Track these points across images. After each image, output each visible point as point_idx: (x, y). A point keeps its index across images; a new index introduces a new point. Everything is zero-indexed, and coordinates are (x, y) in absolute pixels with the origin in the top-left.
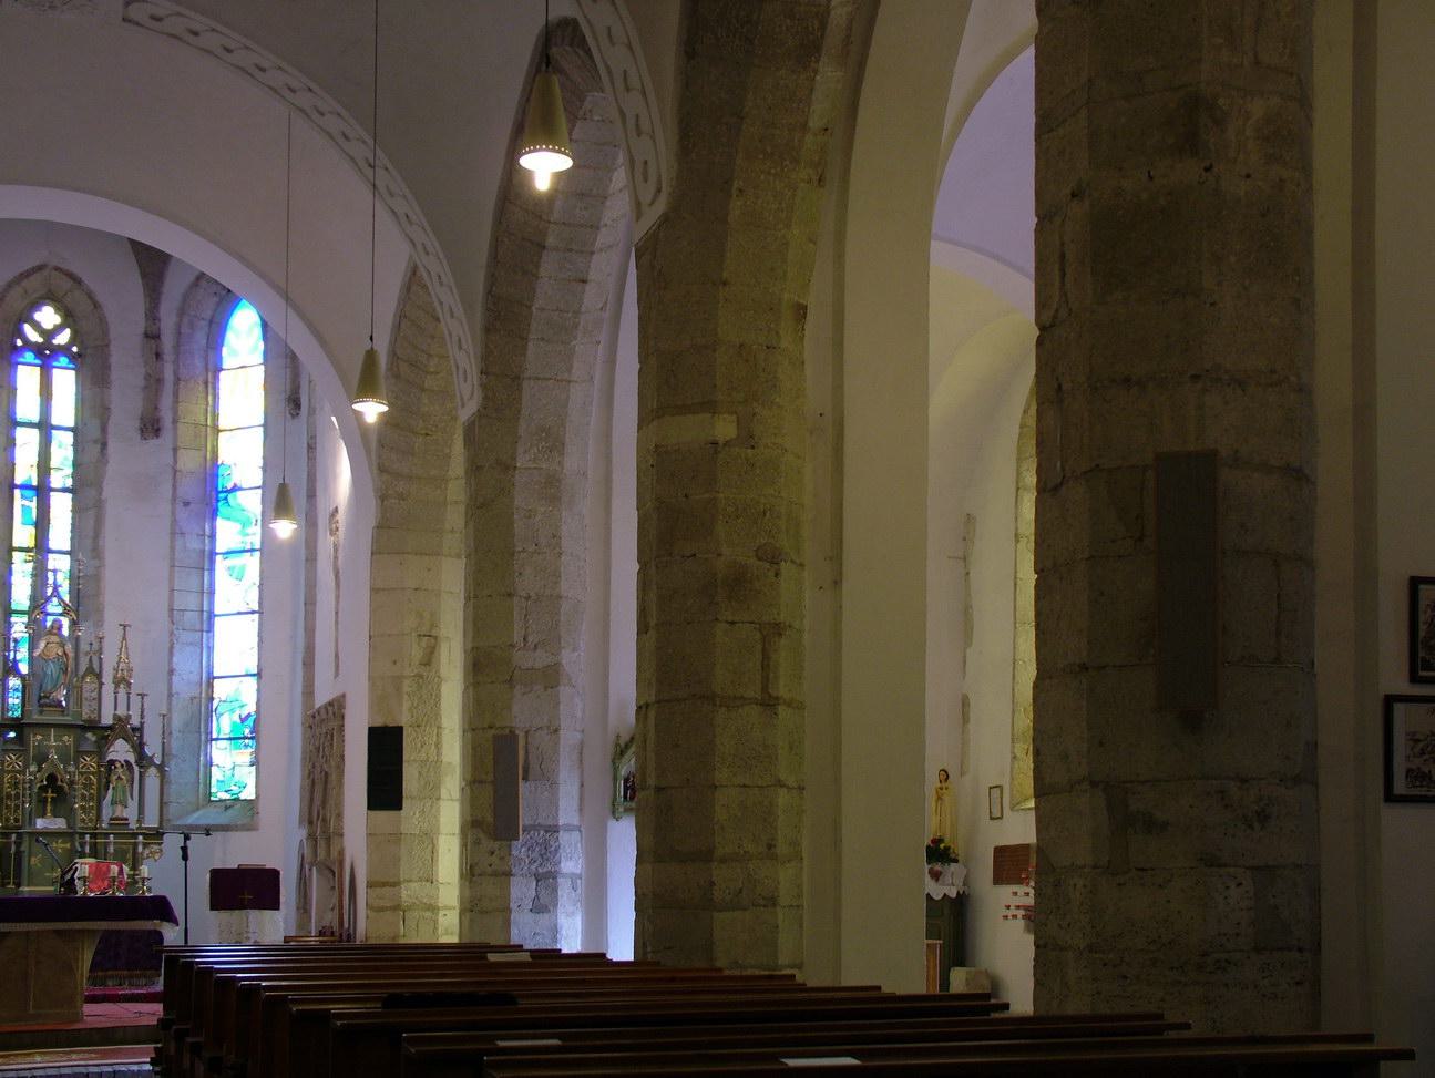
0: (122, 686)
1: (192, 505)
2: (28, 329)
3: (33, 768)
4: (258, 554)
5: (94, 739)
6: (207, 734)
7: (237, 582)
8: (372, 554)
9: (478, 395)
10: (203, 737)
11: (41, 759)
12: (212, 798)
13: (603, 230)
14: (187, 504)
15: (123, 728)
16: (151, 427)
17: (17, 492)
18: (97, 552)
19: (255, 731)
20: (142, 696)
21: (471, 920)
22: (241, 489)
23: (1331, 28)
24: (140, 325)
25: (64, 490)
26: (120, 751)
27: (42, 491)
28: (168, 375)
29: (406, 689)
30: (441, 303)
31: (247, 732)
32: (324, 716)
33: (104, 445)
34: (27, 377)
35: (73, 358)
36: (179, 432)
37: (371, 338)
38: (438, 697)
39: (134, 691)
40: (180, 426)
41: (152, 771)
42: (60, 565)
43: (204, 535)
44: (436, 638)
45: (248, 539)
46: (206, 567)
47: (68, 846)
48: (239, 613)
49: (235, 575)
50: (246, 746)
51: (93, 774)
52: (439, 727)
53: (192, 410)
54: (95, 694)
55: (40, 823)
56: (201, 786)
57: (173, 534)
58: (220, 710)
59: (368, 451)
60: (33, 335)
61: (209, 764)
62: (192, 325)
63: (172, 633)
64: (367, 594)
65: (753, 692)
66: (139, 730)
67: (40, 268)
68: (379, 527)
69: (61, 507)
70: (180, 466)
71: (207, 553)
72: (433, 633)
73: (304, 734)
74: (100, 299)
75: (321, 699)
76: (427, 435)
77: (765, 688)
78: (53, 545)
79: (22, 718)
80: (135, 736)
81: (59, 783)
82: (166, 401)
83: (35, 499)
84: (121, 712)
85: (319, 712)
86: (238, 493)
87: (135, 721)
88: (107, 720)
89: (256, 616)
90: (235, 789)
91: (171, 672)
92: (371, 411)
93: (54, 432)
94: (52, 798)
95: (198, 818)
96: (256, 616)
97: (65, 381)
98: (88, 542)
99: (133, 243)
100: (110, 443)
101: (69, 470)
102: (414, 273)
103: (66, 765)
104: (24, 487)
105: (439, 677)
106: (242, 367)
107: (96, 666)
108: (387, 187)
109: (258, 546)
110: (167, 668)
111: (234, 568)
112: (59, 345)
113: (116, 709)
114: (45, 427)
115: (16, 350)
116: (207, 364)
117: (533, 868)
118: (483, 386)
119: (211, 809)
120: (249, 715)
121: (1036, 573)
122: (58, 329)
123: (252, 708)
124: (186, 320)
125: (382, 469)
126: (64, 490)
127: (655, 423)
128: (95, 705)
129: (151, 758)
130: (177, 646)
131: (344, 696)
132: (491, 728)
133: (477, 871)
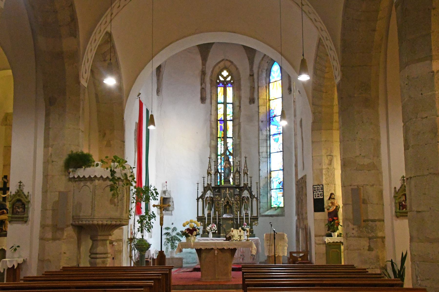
0: (245, 175)
1: (264, 122)
2: (220, 77)
3: (223, 200)
4: (281, 134)
5: (238, 190)
6: (270, 188)
8: (312, 131)
9: (340, 74)
11: (225, 197)
12: (272, 207)
13: (380, 12)
14: (262, 122)
15: (246, 187)
16: (252, 101)
17: (219, 122)
18: (239, 137)
19: (284, 186)
20: (251, 177)
21: (347, 253)
22: (277, 116)
24: (248, 72)
25: (230, 120)
26: (246, 194)
27: (225, 121)
28: (256, 86)
30: (327, 46)
31: (281, 187)
32: (301, 182)
33: (240, 107)
34: (220, 90)
35: (232, 84)
37: (303, 55)
38: (334, 175)
39: (249, 176)
40: (259, 100)
41: (255, 199)
42: (230, 142)
43: (267, 130)
44: (332, 156)
46: (268, 139)
47: (232, 222)
48: (277, 152)
50: (281, 191)
52: (335, 184)
53: (263, 95)
54: (238, 178)
55: (225, 216)
57: (259, 130)
58: (273, 181)
59: (308, 97)
60: (222, 79)
61: (271, 197)
62: (262, 72)
63: (259, 159)
66: (250, 188)
67: (223, 60)
68: (313, 122)
69: (230, 124)
70: (260, 111)
71: (268, 136)
72: (332, 154)
73: (296, 187)
74: (238, 67)
75: (300, 177)
76: (326, 92)
78: (228, 136)
79: (220, 185)
80: (250, 190)
81: (230, 204)
82: (256, 94)
83: (223, 123)
84: (246, 182)
85: (299, 181)
86: (276, 117)
87: (249, 186)
89: (282, 152)
90: (278, 204)
91: (260, 170)
92: (304, 78)
93: (227, 104)
94: (228, 208)
96: (282, 152)
97: (230, 90)
98: (237, 134)
99: (245, 47)
100: (242, 107)
101: (232, 115)
102: (319, 41)
103: (231, 198)
104: (220, 120)
105: (334, 168)
106: (275, 81)
107: (239, 169)
108: (309, 11)
109: (282, 132)
111: (275, 139)
112: (228, 81)
113: (244, 182)
114: (225, 103)
115: (218, 84)
116: (266, 81)
118: (342, 71)
119: (272, 210)
120: (281, 182)
121: (112, 204)
122: (228, 76)
123: (282, 180)
124: (260, 70)
125: (313, 104)
126: (230, 120)
127: (407, 67)
128: (238, 181)
130: (261, 162)
131: (306, 175)
132: (351, 186)
133: (349, 235)
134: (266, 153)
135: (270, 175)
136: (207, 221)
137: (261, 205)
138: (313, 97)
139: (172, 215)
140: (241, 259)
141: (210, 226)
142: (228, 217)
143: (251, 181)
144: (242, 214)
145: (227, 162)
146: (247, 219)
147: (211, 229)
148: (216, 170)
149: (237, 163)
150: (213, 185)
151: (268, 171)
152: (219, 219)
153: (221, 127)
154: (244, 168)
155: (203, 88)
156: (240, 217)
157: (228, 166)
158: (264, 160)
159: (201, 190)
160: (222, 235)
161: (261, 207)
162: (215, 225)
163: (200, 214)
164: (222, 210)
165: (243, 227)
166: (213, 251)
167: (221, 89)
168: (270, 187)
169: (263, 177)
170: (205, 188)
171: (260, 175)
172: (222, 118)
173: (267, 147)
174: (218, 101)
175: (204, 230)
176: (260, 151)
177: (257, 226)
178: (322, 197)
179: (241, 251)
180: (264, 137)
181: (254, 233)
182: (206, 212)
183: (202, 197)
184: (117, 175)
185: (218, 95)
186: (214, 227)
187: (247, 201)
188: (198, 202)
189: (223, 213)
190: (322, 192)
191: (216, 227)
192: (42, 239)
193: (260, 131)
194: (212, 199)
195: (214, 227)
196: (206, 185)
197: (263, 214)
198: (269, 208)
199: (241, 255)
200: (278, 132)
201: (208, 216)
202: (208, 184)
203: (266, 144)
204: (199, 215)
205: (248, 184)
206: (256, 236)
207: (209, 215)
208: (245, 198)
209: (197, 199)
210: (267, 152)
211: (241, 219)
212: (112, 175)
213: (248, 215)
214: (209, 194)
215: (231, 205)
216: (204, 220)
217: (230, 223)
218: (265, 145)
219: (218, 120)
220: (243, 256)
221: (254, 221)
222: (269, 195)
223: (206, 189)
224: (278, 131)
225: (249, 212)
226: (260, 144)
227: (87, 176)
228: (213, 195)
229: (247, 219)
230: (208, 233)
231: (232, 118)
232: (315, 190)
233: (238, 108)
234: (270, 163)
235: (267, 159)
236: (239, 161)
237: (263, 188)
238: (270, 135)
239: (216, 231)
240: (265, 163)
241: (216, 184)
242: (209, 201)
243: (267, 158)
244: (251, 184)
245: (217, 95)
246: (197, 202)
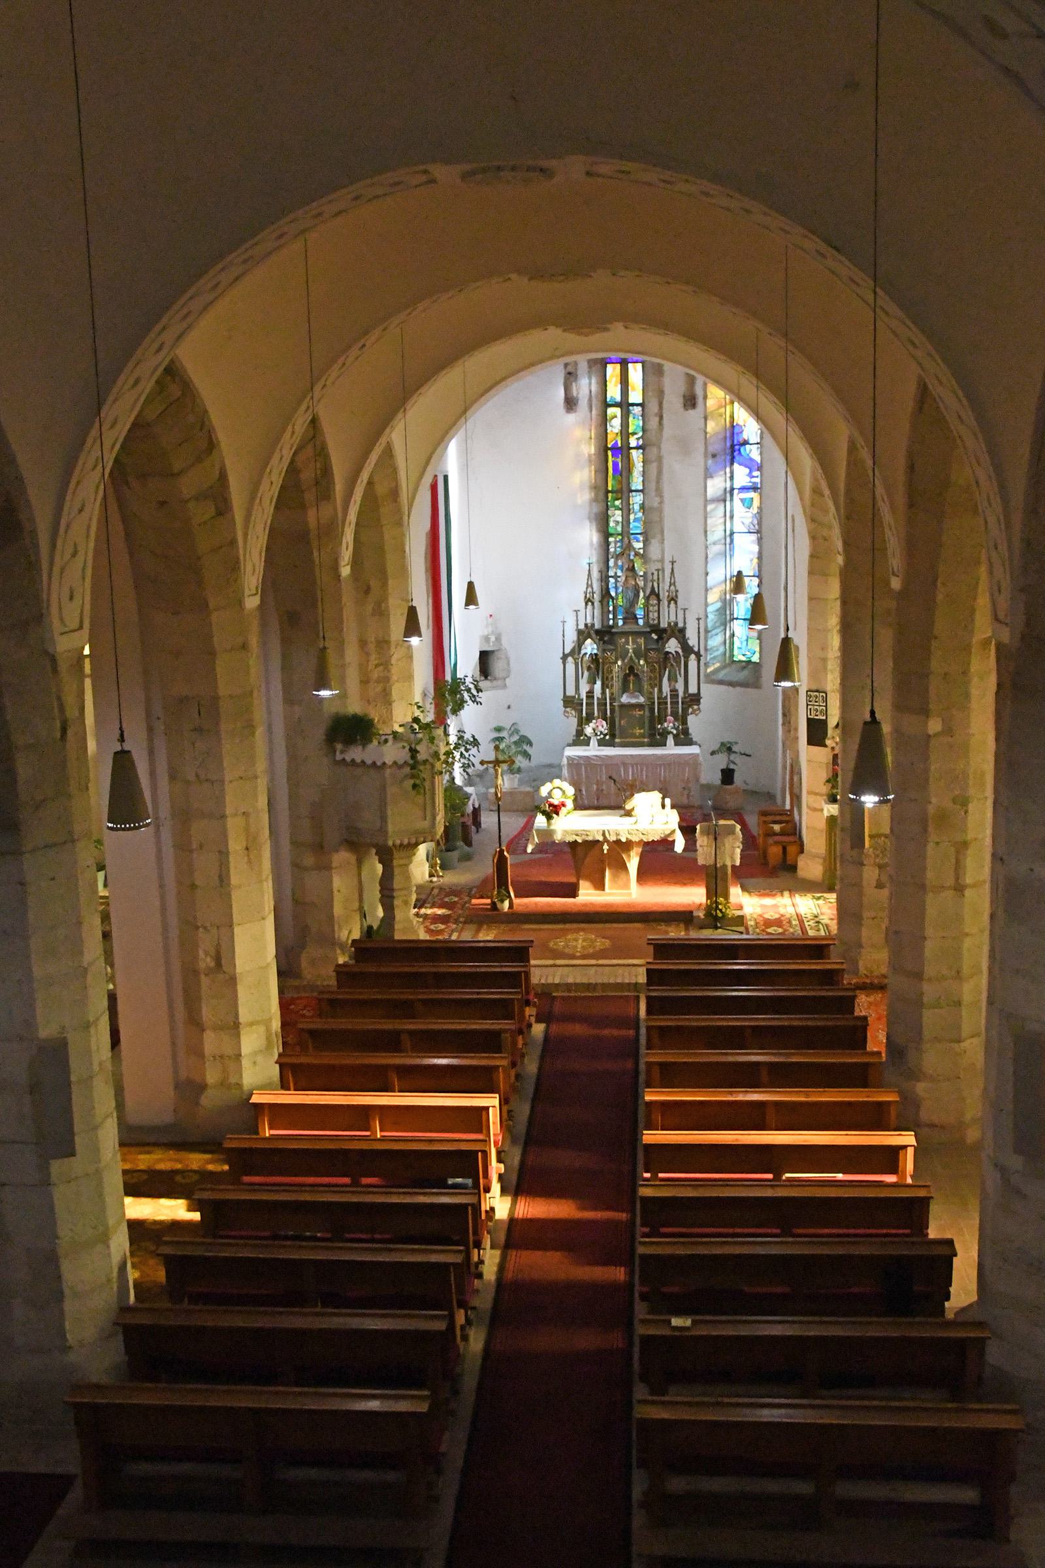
7: (748, 510)
12: (735, 659)
17: (610, 453)
22: (748, 444)
26: (672, 646)
29: (829, 667)
33: (661, 417)
41: (693, 657)
45: (754, 480)
49: (746, 504)
51: (656, 663)
54: (656, 608)
55: (625, 699)
61: (733, 635)
64: (807, 600)
65: (950, 882)
66: (682, 631)
77: (957, 878)
80: (679, 633)
87: (681, 625)
88: (664, 625)
100: (664, 415)
107: (656, 590)
110: (704, 571)
111: (745, 499)
117: (877, 860)
128: (656, 615)
138: (813, 505)
139: (505, 686)
141: (592, 725)
142: (634, 701)
145: (630, 574)
146: (675, 703)
149: (653, 574)
150: (597, 626)
153: (615, 464)
154: (670, 587)
155: (570, 373)
156: (658, 698)
159: (571, 638)
162: (604, 723)
163: (571, 692)
164: (617, 684)
166: (599, 845)
167: (614, 369)
168: (732, 614)
170: (580, 632)
172: (616, 443)
174: (608, 400)
175: (580, 728)
178: (824, 718)
182: (584, 688)
183: (572, 653)
184: (421, 757)
185: (608, 383)
186: (600, 728)
187: (674, 664)
190: (824, 708)
192: (296, 865)
194: (595, 659)
195: (600, 728)
196: (582, 627)
198: (727, 661)
200: (751, 484)
201: (587, 697)
202: (586, 625)
204: (568, 694)
207: (590, 694)
208: (671, 656)
211: (662, 702)
212: (413, 757)
214: (590, 647)
221: (690, 706)
223: (582, 636)
224: (751, 482)
227: (369, 762)
229: (675, 703)
230: (589, 738)
232: (810, 701)
233: (657, 419)
236: (658, 570)
238: (732, 489)
241: (605, 624)
245: (606, 386)
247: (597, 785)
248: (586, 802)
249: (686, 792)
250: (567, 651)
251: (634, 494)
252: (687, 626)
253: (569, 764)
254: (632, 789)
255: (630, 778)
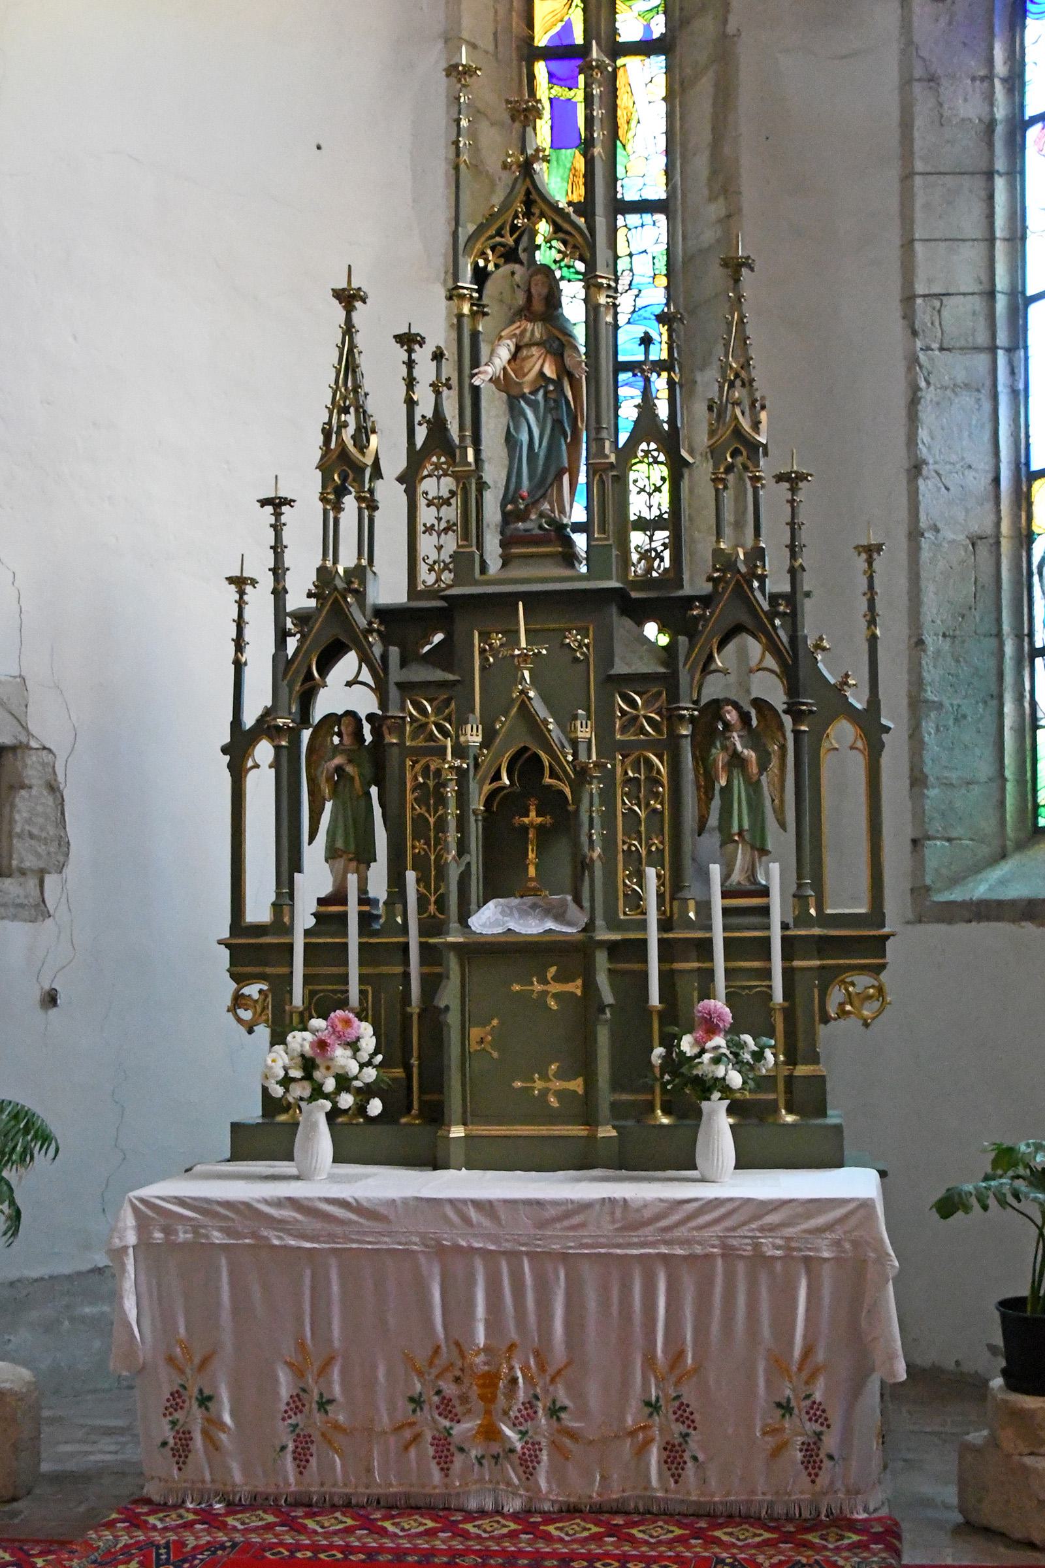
6: (1019, 637)
10: (1009, 649)
17: (541, 69)
23: (3, 1385)
25: (645, 48)
36: (942, 316)
41: (843, 732)
43: (989, 77)
46: (1000, 164)
47: (575, 987)
51: (652, 745)
56: (1010, 787)
63: (913, 361)
87: (778, 583)
91: (916, 469)
95: (1003, 882)
103: (567, 721)
107: (663, 411)
126: (645, 48)
129: (839, 690)
130: (929, 395)
134: (977, 303)
135: (1016, 518)
136: (307, 979)
137: (928, 805)
139: (39, 910)
140: (654, 1455)
142: (532, 927)
143: (794, 526)
144: (693, 892)
145: (536, 330)
147: (308, 1077)
148: (421, 433)
151: (996, 481)
152: (429, 954)
156: (665, 925)
157: (541, 374)
158: (961, 376)
160: (457, 1132)
161: (936, 827)
163: (258, 911)
165: (687, 1045)
169: (948, 534)
171: (922, 516)
172: (568, 27)
173: (991, 240)
176: (920, 289)
177: (876, 1026)
179: (649, 1360)
180: (965, 149)
181: (834, 1117)
186: (342, 1057)
187: (750, 754)
188: (238, 772)
189: (475, 888)
191: (368, 1043)
193: (917, 88)
195: (342, 1057)
197: (956, 895)
199: (653, 1407)
203: (977, 209)
205: (757, 554)
206: (848, 1153)
208: (732, 716)
209: (225, 750)
210: (991, 294)
213: (765, 911)
215: (567, 791)
216: (399, 970)
217: (553, 1101)
218: (969, 222)
219: (530, 53)
220: (684, 1414)
221: (828, 976)
222: (1009, 708)
225: (775, 868)
226: (919, 215)
228: (380, 690)
231: (658, 27)
234: (1020, 396)
235: (983, 359)
237: (946, 646)
239: (366, 1093)
240: (966, 399)
242: (338, 760)
243: (993, 349)
244: (793, 556)
246: (226, 778)
247: (298, 1372)
248: (238, 1477)
249: (798, 1429)
250: (249, 720)
251: (633, 219)
252: (808, 583)
253: (144, 1246)
254: (489, 1399)
255: (481, 1339)
